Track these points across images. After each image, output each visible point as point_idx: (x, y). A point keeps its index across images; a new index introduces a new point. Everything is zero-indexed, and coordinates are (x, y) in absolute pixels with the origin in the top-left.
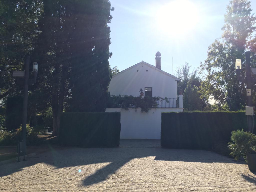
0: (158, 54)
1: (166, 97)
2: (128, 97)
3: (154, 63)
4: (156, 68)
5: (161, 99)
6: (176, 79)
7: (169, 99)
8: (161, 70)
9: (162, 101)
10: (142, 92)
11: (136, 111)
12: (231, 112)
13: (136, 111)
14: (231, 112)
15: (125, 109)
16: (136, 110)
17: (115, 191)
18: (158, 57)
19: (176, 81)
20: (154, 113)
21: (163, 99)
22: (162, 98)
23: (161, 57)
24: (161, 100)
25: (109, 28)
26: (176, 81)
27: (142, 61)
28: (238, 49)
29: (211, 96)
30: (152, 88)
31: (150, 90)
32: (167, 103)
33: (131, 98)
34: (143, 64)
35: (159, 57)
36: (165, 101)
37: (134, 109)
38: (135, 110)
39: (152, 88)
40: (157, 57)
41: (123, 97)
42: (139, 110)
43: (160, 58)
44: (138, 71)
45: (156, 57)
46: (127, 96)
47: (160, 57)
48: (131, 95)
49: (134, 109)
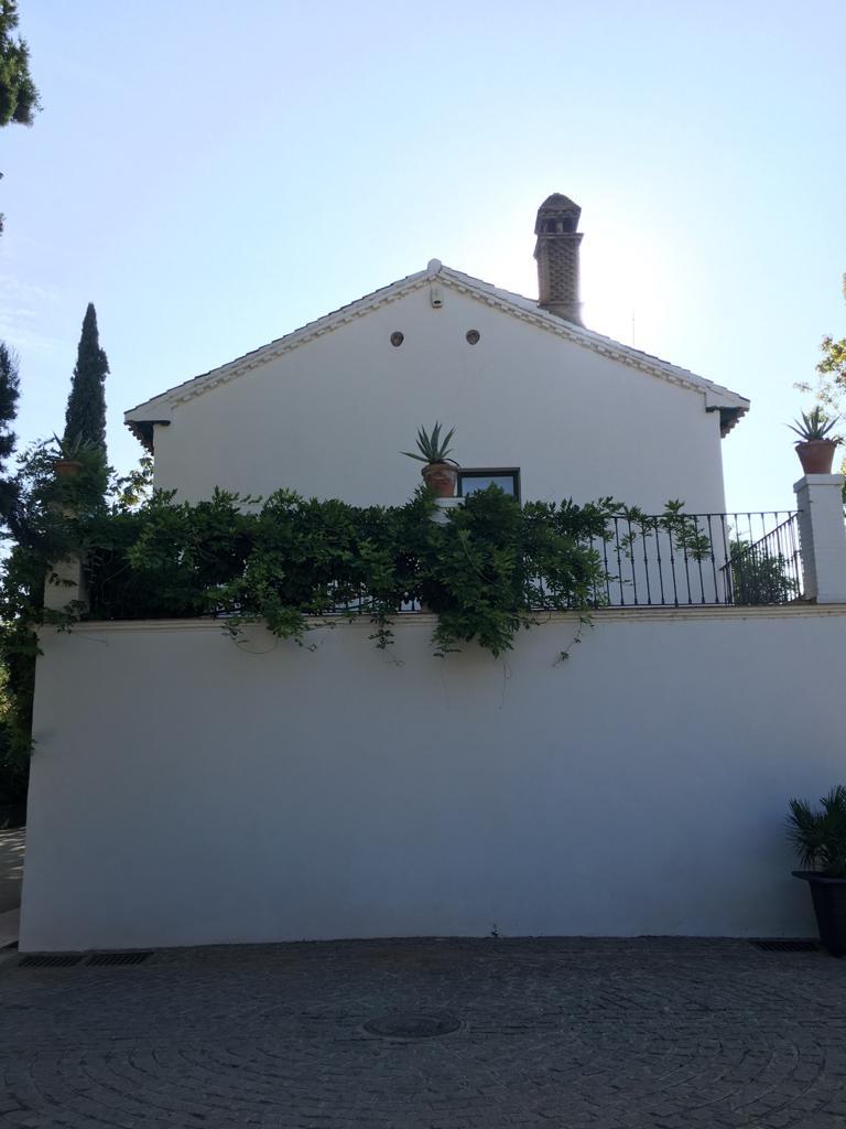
1: (674, 506)
2: (302, 507)
3: (521, 278)
4: (546, 314)
5: (623, 527)
6: (710, 395)
7: (702, 523)
9: (638, 543)
10: (441, 462)
11: (383, 639)
13: (383, 639)
15: (485, 642)
16: (382, 634)
19: (710, 410)
20: (565, 656)
21: (648, 523)
22: (633, 515)
24: (631, 536)
26: (710, 410)
27: (434, 263)
30: (514, 473)
32: (693, 562)
33: (326, 519)
34: (439, 283)
36: (665, 539)
37: (363, 620)
38: (374, 629)
39: (514, 473)
41: (404, 606)
42: (415, 627)
44: (397, 339)
46: (291, 500)
48: (333, 498)
49: (366, 629)
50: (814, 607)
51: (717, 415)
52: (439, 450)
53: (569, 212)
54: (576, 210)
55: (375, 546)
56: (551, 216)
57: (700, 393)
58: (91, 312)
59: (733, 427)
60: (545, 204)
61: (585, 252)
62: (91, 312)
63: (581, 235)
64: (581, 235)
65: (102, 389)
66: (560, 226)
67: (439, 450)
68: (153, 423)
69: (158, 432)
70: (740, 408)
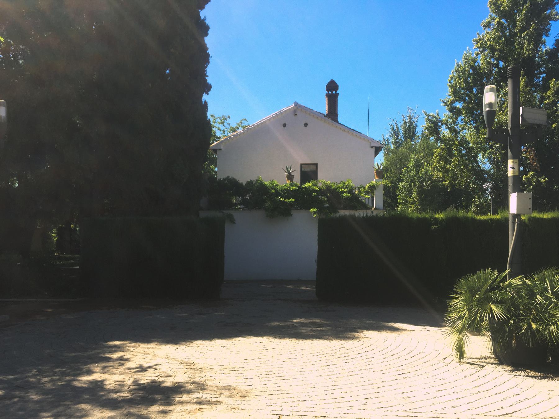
0: (332, 87)
8: (337, 122)
12: (546, 216)
14: (546, 216)
17: (558, 284)
18: (332, 92)
19: (372, 147)
23: (337, 92)
25: (206, 22)
26: (372, 147)
28: (95, 31)
29: (77, 230)
30: (316, 165)
31: (313, 168)
35: (334, 92)
39: (316, 165)
40: (334, 92)
43: (337, 95)
45: (326, 92)
47: (336, 92)
60: (328, 84)
69: (218, 152)
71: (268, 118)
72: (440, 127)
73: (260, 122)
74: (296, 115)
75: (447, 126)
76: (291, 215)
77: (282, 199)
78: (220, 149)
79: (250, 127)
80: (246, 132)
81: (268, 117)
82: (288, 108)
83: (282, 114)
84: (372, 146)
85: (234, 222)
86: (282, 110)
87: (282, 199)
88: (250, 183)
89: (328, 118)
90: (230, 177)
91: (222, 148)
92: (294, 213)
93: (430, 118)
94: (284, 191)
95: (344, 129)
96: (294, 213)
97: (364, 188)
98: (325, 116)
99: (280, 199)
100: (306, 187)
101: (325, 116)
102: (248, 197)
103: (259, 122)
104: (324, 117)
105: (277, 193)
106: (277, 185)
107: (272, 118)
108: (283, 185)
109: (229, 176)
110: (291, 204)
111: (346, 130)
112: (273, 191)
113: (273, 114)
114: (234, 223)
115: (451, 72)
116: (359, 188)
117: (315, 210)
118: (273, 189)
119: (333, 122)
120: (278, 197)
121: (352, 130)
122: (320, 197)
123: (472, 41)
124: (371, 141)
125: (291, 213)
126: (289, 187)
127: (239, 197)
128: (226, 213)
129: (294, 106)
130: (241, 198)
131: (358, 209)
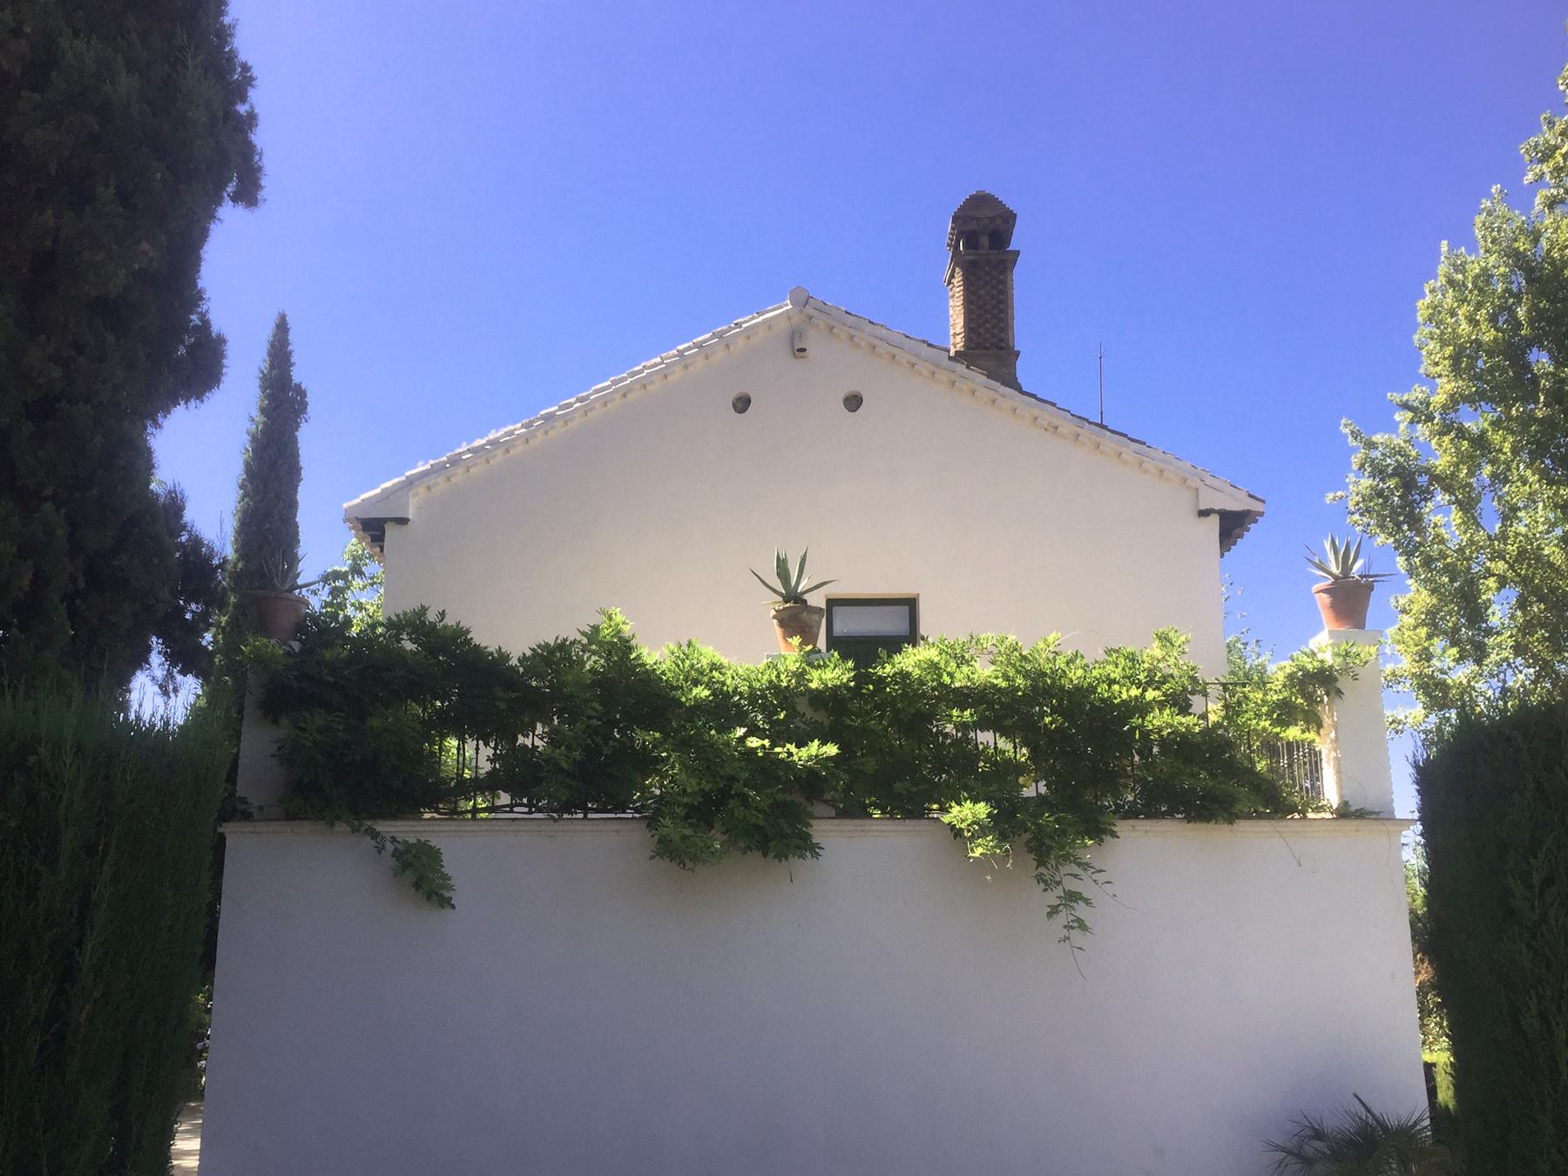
8: (1019, 388)
19: (1204, 513)
26: (1204, 513)
30: (911, 604)
39: (911, 604)
50: (418, 823)
51: (1214, 520)
52: (793, 583)
53: (998, 221)
54: (1010, 218)
55: (647, 737)
56: (973, 226)
57: (1189, 487)
58: (282, 327)
59: (1241, 536)
60: (962, 208)
61: (1022, 281)
62: (282, 327)
63: (1017, 253)
64: (1017, 253)
65: (295, 441)
66: (985, 241)
67: (793, 583)
68: (385, 520)
69: (391, 532)
70: (1249, 512)
71: (656, 365)
72: (1427, 495)
73: (614, 383)
74: (803, 350)
75: (1451, 494)
76: (805, 846)
77: (753, 742)
78: (403, 521)
79: (561, 408)
80: (540, 434)
81: (658, 360)
82: (761, 318)
83: (727, 346)
84: (1202, 508)
85: (446, 894)
86: (731, 329)
87: (753, 742)
88: (553, 657)
89: (968, 367)
90: (431, 617)
91: (411, 514)
92: (827, 832)
93: (1376, 454)
94: (764, 697)
95: (1056, 422)
96: (827, 832)
97: (1262, 684)
98: (950, 358)
99: (742, 740)
100: (904, 675)
101: (950, 358)
102: (535, 740)
103: (608, 383)
104: (946, 362)
105: (724, 708)
106: (714, 667)
107: (678, 368)
108: (761, 666)
109: (424, 610)
110: (811, 781)
111: (1067, 426)
112: (702, 692)
113: (681, 347)
114: (446, 903)
115: (1423, 288)
116: (1225, 690)
117: (982, 810)
118: (696, 683)
119: (997, 385)
120: (725, 728)
121: (1093, 427)
122: (985, 738)
123: (1540, 121)
124: (1199, 484)
125: (809, 836)
126: (800, 676)
127: (486, 744)
128: (394, 839)
129: (790, 307)
130: (495, 749)
131: (1238, 817)
